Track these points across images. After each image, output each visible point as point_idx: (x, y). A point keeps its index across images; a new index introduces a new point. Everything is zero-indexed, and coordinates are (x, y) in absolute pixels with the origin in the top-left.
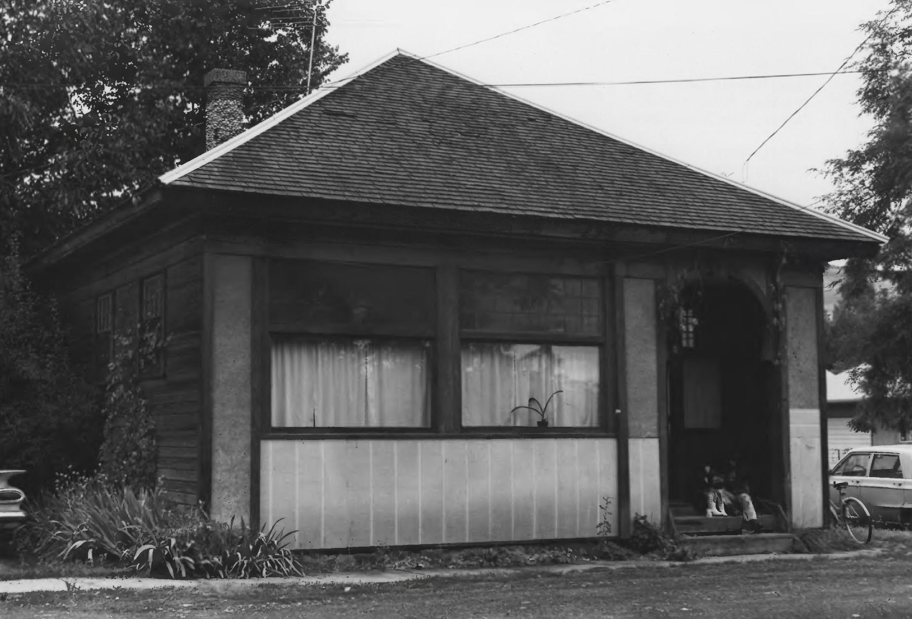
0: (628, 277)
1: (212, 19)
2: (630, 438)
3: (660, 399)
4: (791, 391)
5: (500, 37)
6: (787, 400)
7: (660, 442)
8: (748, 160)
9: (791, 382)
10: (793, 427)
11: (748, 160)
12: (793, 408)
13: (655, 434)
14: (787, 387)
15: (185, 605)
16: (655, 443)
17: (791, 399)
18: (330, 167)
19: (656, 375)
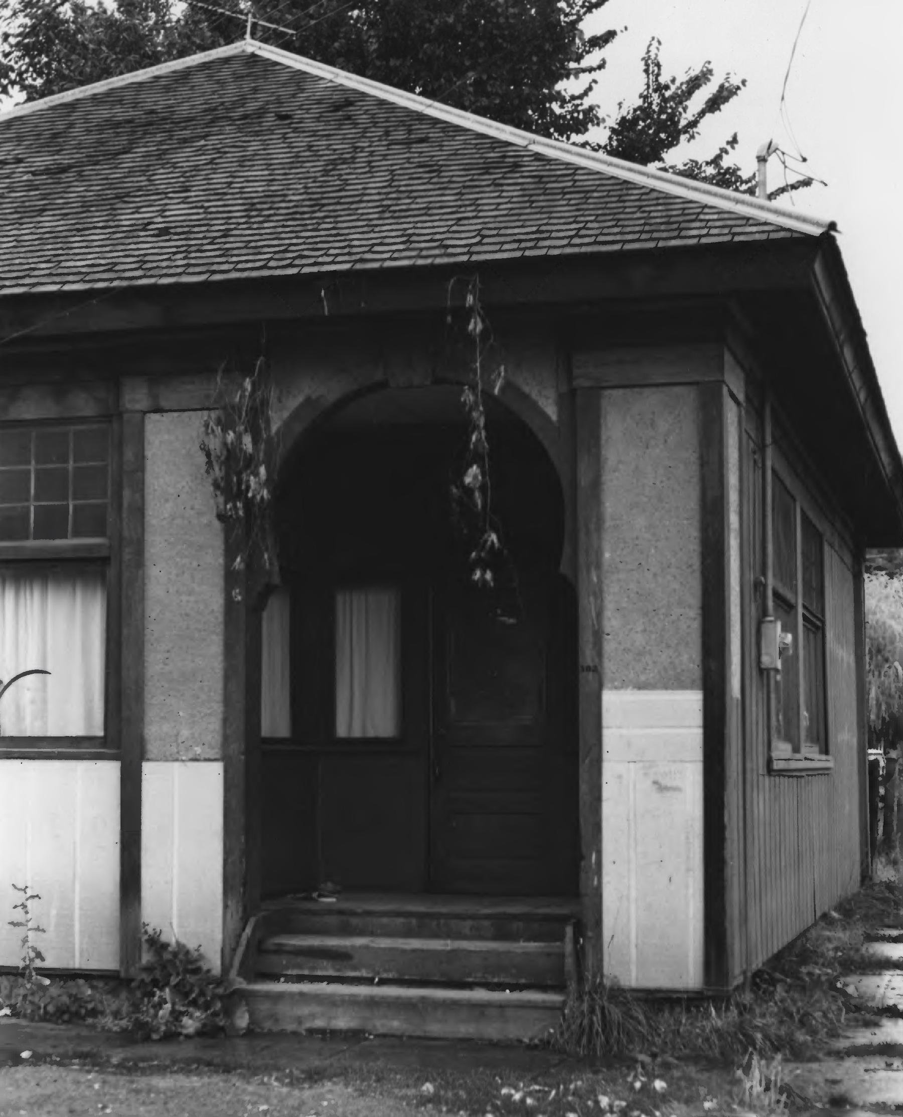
0: (158, 410)
1: (559, 63)
2: (148, 760)
3: (728, 503)
4: (609, 646)
5: (809, 13)
6: (597, 670)
7: (226, 771)
8: (783, 98)
9: (612, 622)
10: (611, 737)
11: (783, 98)
12: (611, 689)
13: (215, 753)
14: (598, 636)
15: (595, 579)
16: (217, 769)
17: (609, 667)
18: (185, 224)
19: (221, 618)
